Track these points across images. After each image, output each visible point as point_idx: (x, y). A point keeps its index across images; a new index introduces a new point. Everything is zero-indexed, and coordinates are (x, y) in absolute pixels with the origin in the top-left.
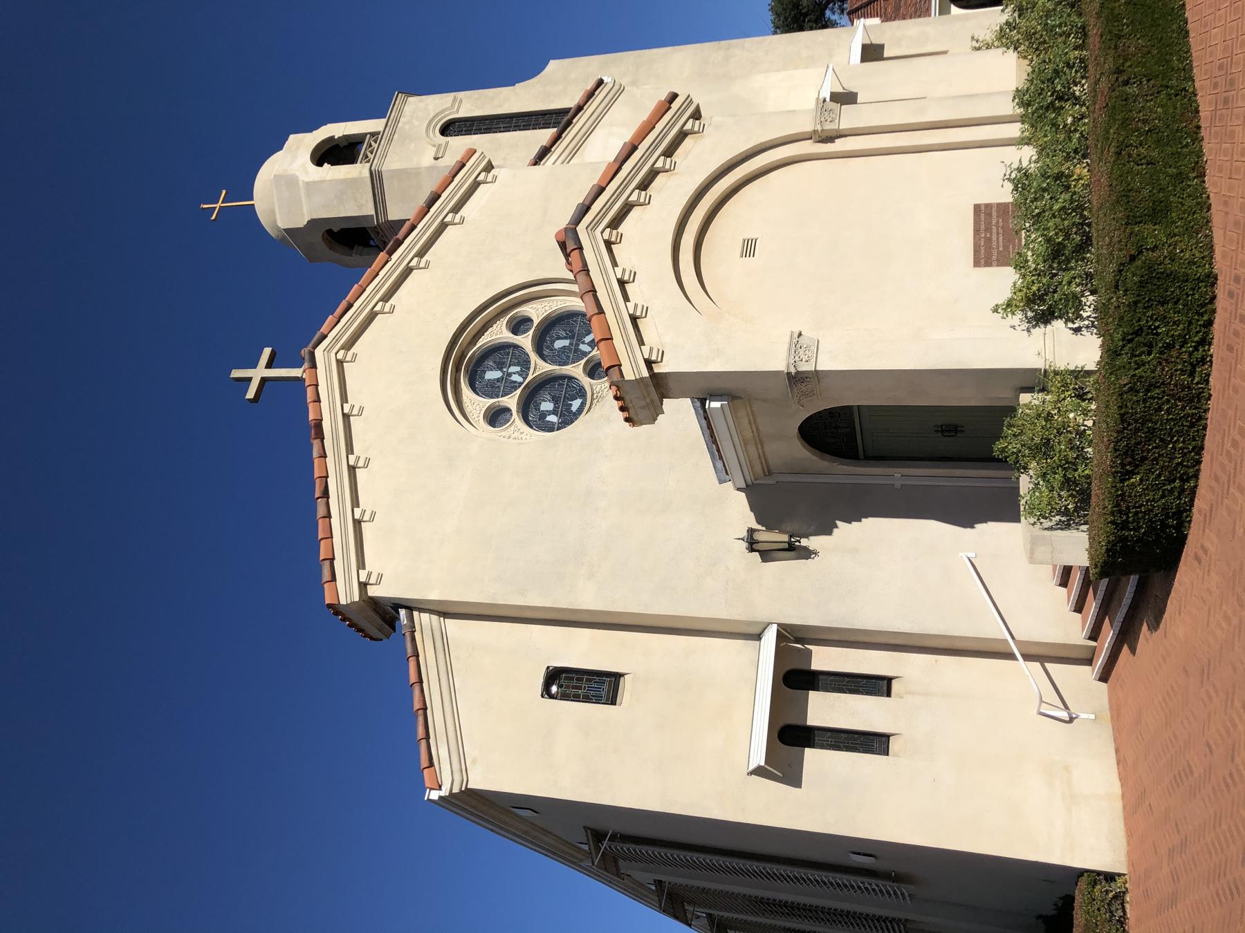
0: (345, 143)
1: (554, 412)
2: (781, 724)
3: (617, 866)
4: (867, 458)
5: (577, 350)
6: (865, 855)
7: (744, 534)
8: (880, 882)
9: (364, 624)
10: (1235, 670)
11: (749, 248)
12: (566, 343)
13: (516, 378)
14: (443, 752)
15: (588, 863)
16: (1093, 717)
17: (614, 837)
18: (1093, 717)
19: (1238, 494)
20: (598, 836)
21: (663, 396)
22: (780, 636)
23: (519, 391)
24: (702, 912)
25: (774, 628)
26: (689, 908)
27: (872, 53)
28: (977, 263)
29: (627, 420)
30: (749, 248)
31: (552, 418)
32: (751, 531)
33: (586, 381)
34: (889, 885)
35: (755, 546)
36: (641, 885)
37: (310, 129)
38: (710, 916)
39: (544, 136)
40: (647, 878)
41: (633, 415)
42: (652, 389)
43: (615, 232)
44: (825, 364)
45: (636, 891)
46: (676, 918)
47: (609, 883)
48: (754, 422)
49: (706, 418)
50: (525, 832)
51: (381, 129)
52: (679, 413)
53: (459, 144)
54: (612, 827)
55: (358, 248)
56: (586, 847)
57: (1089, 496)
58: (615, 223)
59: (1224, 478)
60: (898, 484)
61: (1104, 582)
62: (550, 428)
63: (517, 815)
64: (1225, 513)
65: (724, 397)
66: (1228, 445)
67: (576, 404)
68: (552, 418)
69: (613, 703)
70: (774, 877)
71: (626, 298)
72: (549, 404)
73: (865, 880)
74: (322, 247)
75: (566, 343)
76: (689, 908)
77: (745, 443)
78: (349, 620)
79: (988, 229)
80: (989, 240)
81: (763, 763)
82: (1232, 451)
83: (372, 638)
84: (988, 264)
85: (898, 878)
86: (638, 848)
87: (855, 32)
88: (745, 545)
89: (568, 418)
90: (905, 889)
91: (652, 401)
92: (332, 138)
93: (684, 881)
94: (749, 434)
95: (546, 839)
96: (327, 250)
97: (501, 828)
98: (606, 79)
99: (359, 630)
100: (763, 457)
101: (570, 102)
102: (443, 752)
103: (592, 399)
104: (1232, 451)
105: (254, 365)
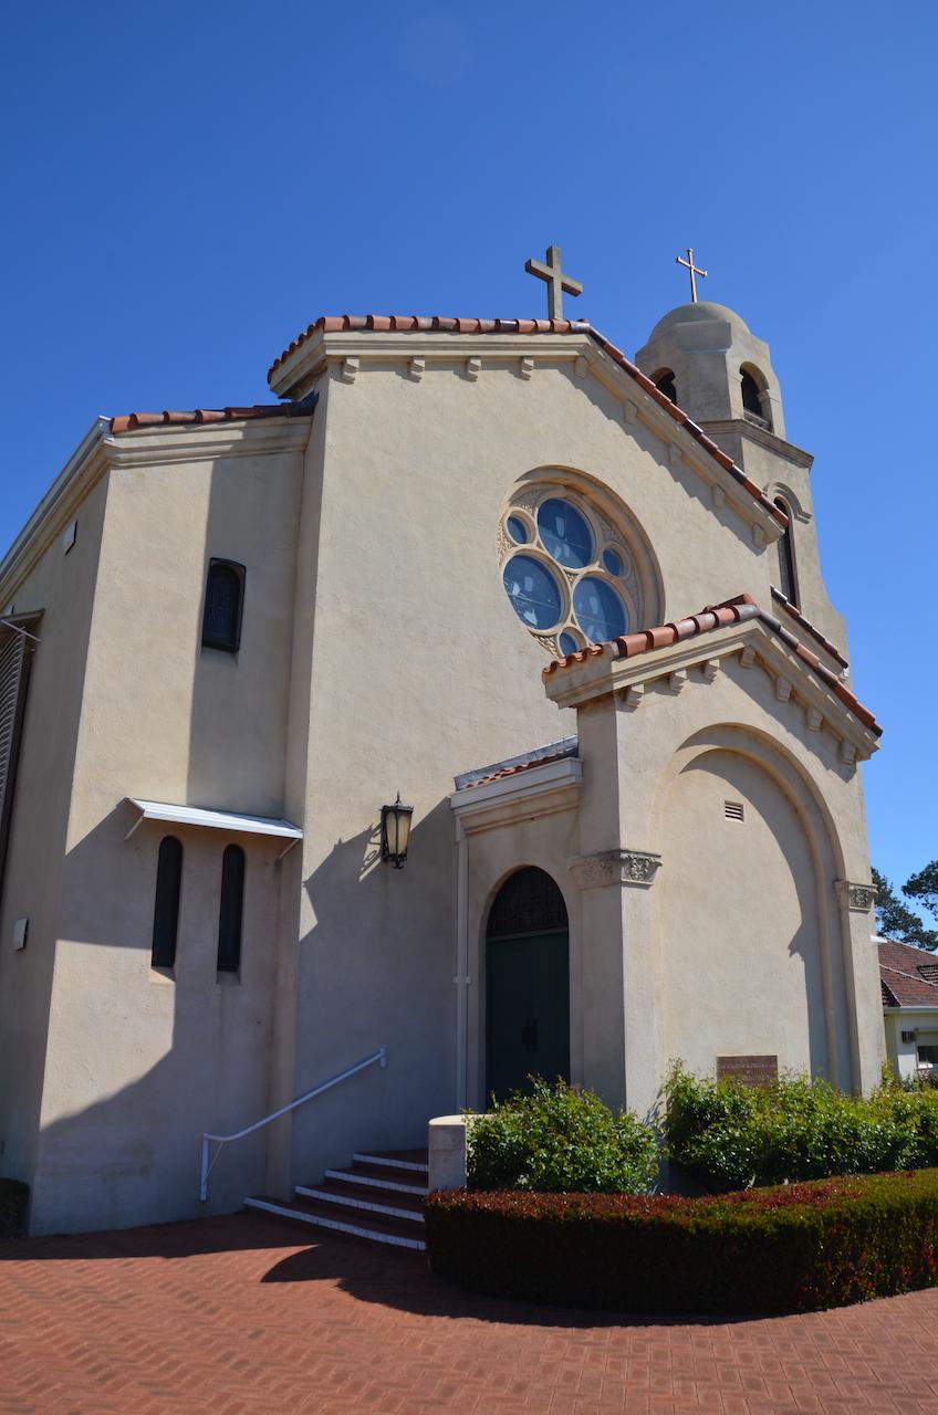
0: (761, 400)
2: (183, 840)
6: (26, 936)
7: (404, 804)
9: (292, 362)
14: (153, 441)
16: (203, 1198)
17: (30, 644)
18: (203, 1198)
21: (580, 707)
23: (546, 552)
28: (722, 1061)
29: (554, 665)
32: (408, 813)
37: (774, 364)
41: (559, 671)
42: (595, 693)
43: (751, 662)
44: (627, 894)
48: (544, 814)
49: (546, 760)
50: (36, 541)
51: (776, 435)
52: (561, 726)
54: (48, 642)
65: (582, 775)
72: (535, 590)
78: (300, 345)
81: (145, 815)
83: (272, 371)
88: (391, 802)
91: (576, 694)
92: (766, 386)
95: (23, 567)
97: (45, 513)
98: (846, 671)
99: (285, 356)
100: (493, 826)
102: (153, 441)
103: (539, 636)
105: (564, 272)
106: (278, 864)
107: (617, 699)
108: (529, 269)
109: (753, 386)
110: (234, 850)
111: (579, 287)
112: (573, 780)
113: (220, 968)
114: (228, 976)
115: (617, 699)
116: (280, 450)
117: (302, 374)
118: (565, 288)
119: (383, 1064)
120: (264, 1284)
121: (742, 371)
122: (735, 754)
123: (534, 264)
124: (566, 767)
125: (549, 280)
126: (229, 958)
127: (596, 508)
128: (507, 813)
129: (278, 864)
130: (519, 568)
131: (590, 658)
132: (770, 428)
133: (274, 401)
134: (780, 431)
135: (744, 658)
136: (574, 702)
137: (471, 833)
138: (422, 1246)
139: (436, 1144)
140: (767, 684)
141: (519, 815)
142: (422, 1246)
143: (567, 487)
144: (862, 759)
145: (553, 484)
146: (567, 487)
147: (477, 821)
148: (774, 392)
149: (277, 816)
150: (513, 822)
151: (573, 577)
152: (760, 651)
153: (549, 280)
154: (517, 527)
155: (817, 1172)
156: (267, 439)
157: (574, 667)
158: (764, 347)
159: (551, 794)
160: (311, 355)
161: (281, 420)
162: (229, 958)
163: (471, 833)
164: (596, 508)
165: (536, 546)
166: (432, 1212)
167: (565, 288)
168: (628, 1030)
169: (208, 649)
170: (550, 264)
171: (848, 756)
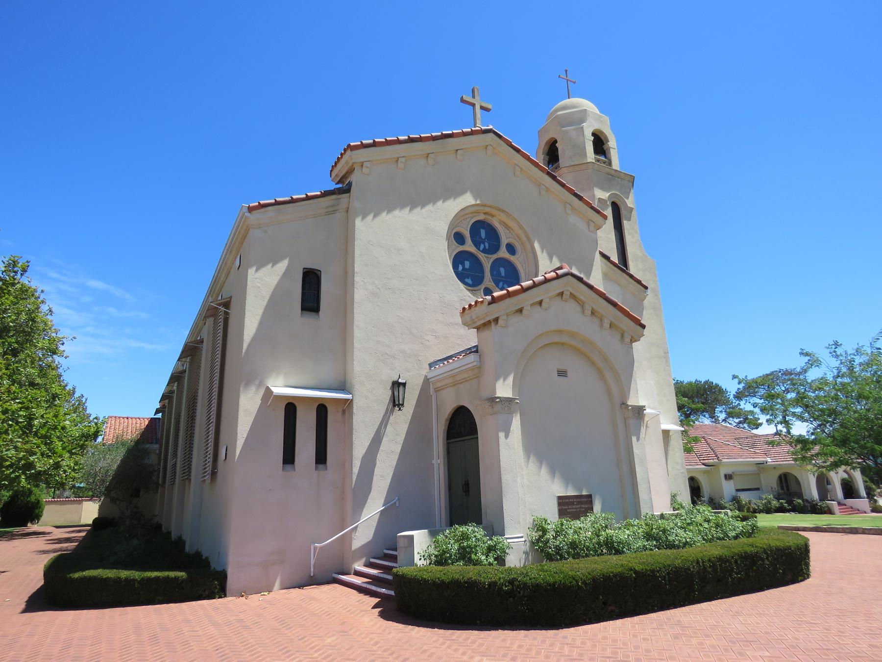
1: (464, 268)
3: (211, 316)
4: (448, 444)
5: (500, 281)
8: (211, 464)
9: (343, 161)
10: (348, 649)
11: (562, 373)
12: (503, 274)
13: (482, 246)
15: (210, 299)
17: (226, 313)
19: (446, 645)
20: (227, 305)
21: (478, 328)
22: (347, 400)
24: (186, 366)
25: (349, 397)
26: (188, 359)
27: (666, 433)
29: (464, 309)
30: (562, 373)
31: (460, 268)
33: (482, 287)
34: (209, 469)
35: (396, 386)
36: (200, 332)
38: (184, 371)
39: (615, 258)
40: (205, 334)
41: (466, 312)
42: (482, 322)
45: (196, 329)
46: (183, 352)
47: (200, 313)
53: (609, 212)
54: (233, 312)
55: (547, 158)
56: (220, 298)
57: (442, 565)
58: (573, 296)
59: (475, 646)
60: (434, 462)
61: (390, 577)
62: (455, 267)
63: (235, 259)
64: (434, 639)
66: (480, 641)
67: (469, 281)
68: (460, 268)
69: (302, 309)
70: (210, 405)
71: (532, 305)
72: (467, 269)
73: (211, 456)
74: (547, 138)
75: (503, 274)
76: (188, 359)
77: (453, 376)
79: (579, 503)
80: (572, 503)
82: (470, 641)
84: (560, 504)
85: (214, 474)
86: (222, 324)
87: (675, 424)
89: (461, 277)
90: (208, 478)
91: (475, 323)
93: (204, 352)
94: (458, 378)
96: (545, 142)
99: (336, 164)
101: (632, 270)
104: (470, 641)
106: (344, 411)
107: (493, 324)
108: (463, 101)
109: (600, 144)
110: (322, 409)
111: (490, 106)
112: (475, 364)
113: (316, 463)
114: (321, 466)
115: (493, 324)
116: (334, 212)
117: (344, 172)
118: (482, 108)
119: (397, 504)
120: (28, 615)
121: (594, 134)
122: (563, 344)
123: (465, 98)
124: (472, 357)
125: (473, 105)
126: (321, 458)
127: (501, 222)
128: (451, 380)
129: (344, 411)
130: (458, 260)
131: (478, 305)
132: (610, 164)
133: (332, 186)
134: (616, 165)
135: (543, 304)
136: (475, 325)
137: (437, 390)
138: (392, 593)
139: (401, 544)
140: (578, 308)
141: (456, 381)
142: (392, 593)
143: (485, 213)
144: (635, 341)
145: (477, 212)
146: (485, 213)
147: (439, 384)
148: (612, 143)
149: (342, 388)
150: (455, 384)
151: (487, 261)
152: (574, 292)
153: (473, 105)
154: (459, 238)
155: (678, 547)
156: (328, 207)
157: (473, 309)
158: (607, 119)
159: (467, 370)
160: (346, 163)
161: (334, 197)
162: (321, 458)
163: (437, 390)
164: (501, 222)
165: (469, 247)
166: (396, 576)
167: (482, 108)
168: (504, 485)
169: (304, 312)
170: (474, 97)
171: (627, 340)
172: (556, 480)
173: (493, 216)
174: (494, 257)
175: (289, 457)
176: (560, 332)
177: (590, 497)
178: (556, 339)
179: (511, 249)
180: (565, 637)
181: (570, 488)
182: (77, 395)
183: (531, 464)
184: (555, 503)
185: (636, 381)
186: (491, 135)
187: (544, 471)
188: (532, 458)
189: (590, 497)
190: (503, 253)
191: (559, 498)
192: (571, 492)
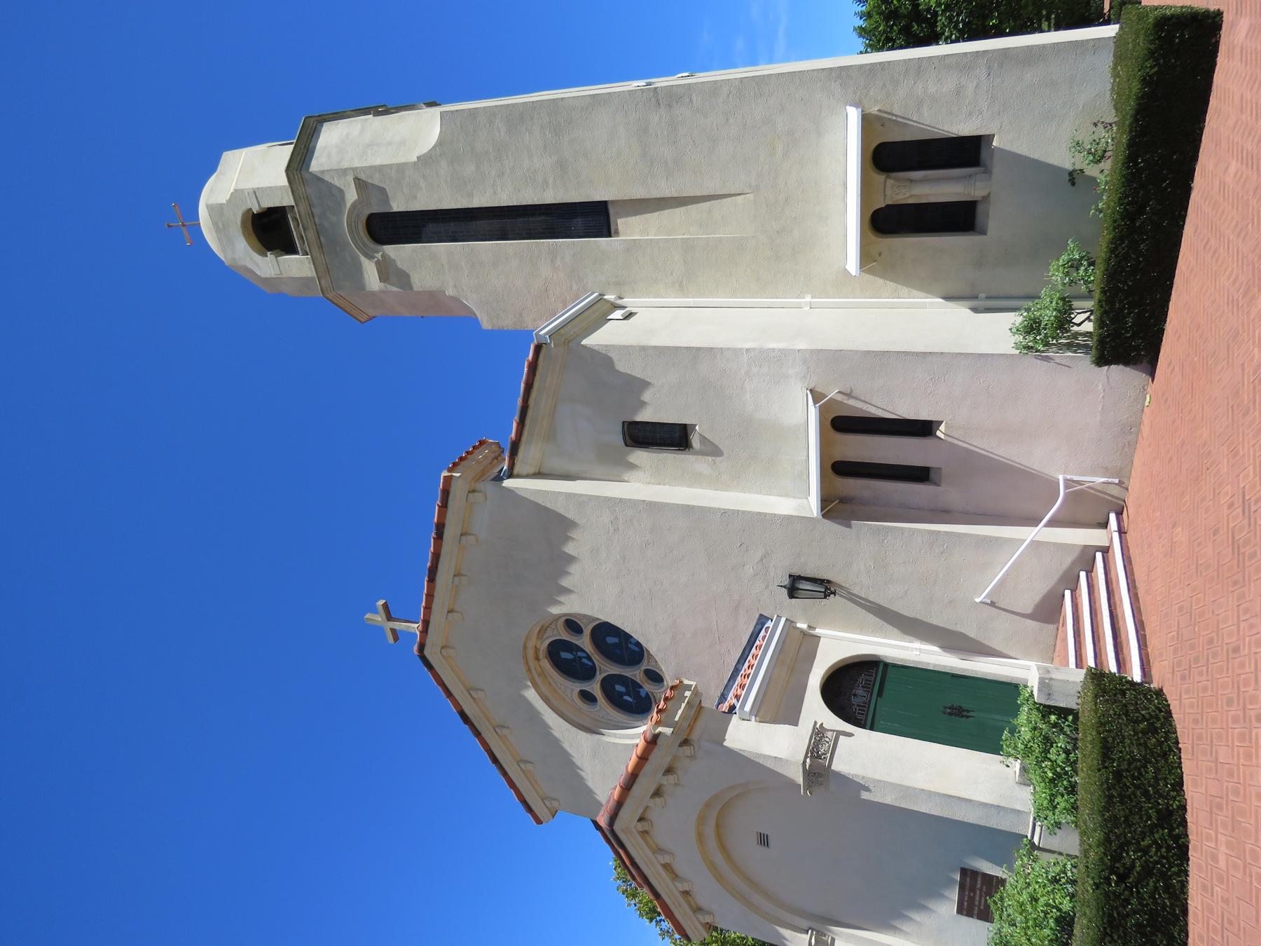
11: (764, 840)
30: (764, 840)
79: (973, 889)
84: (970, 914)
122: (718, 826)
151: (606, 668)
172: (931, 906)
173: (536, 650)
174: (599, 677)
175: (920, 475)
176: (701, 837)
177: (964, 872)
178: (712, 844)
179: (587, 697)
180: (1201, 938)
181: (946, 893)
182: (861, 23)
183: (904, 928)
184: (965, 920)
185: (766, 757)
186: (427, 652)
187: (917, 916)
188: (897, 924)
189: (964, 872)
190: (595, 687)
191: (960, 911)
192: (954, 895)
